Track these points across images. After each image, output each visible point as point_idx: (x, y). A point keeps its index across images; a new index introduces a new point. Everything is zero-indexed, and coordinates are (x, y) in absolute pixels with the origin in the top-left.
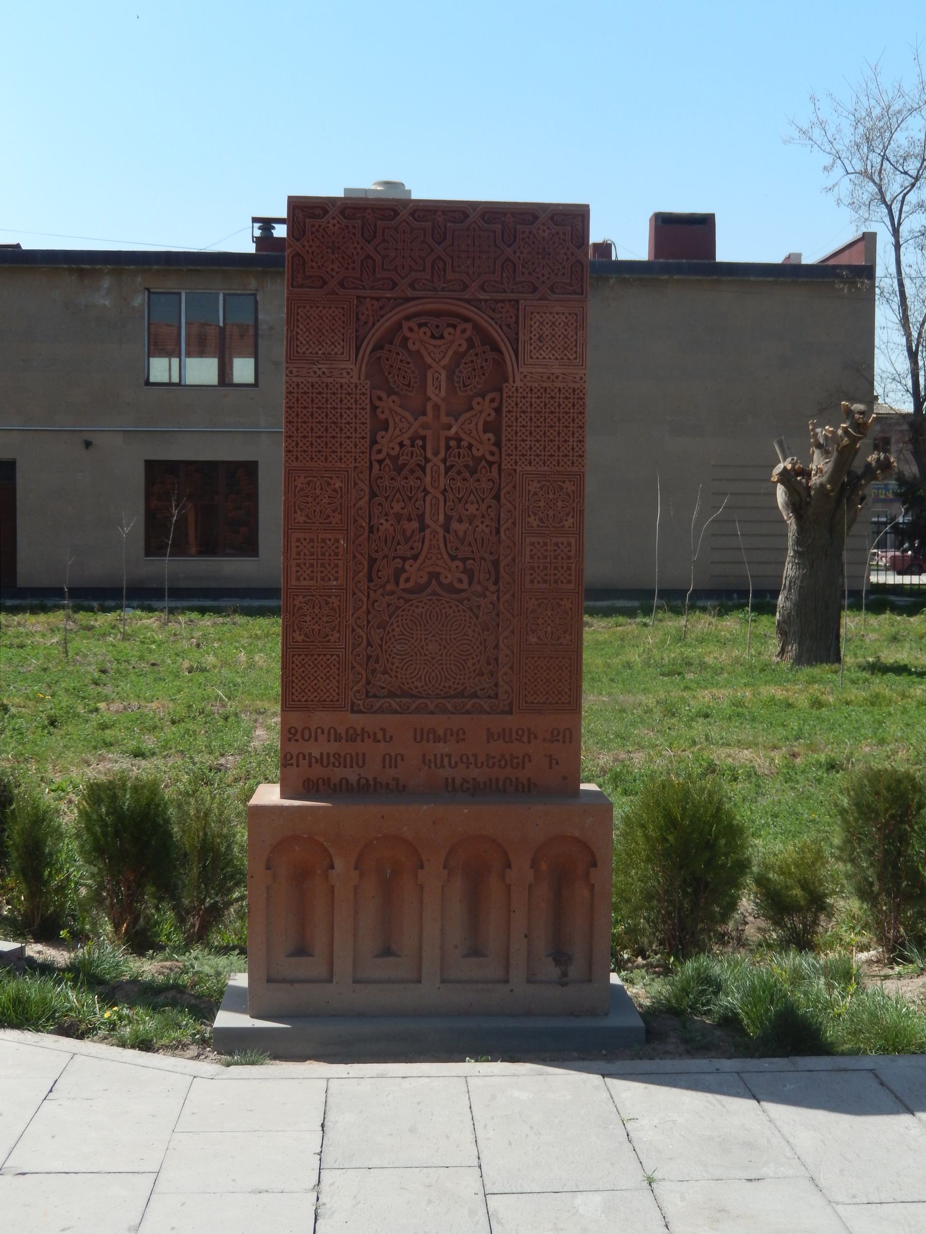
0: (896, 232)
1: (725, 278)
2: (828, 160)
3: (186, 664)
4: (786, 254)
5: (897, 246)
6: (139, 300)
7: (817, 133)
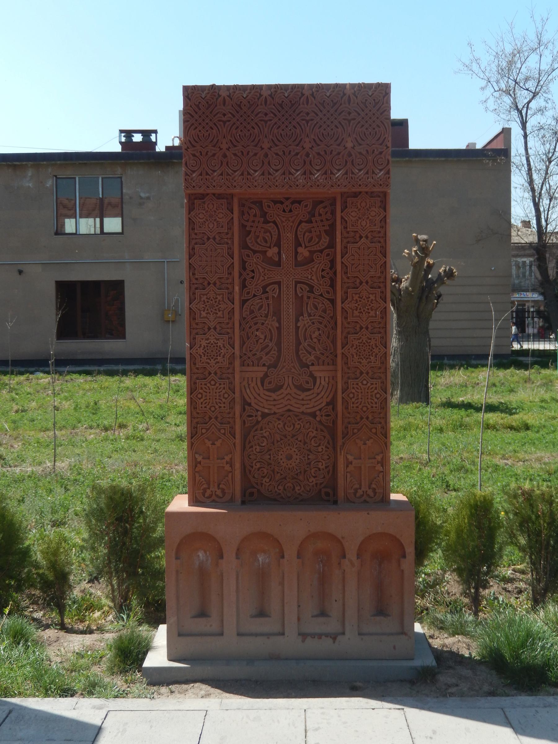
0: (524, 125)
1: (414, 159)
2: (484, 83)
3: (15, 408)
4: (467, 144)
5: (525, 136)
6: (50, 183)
7: (475, 67)
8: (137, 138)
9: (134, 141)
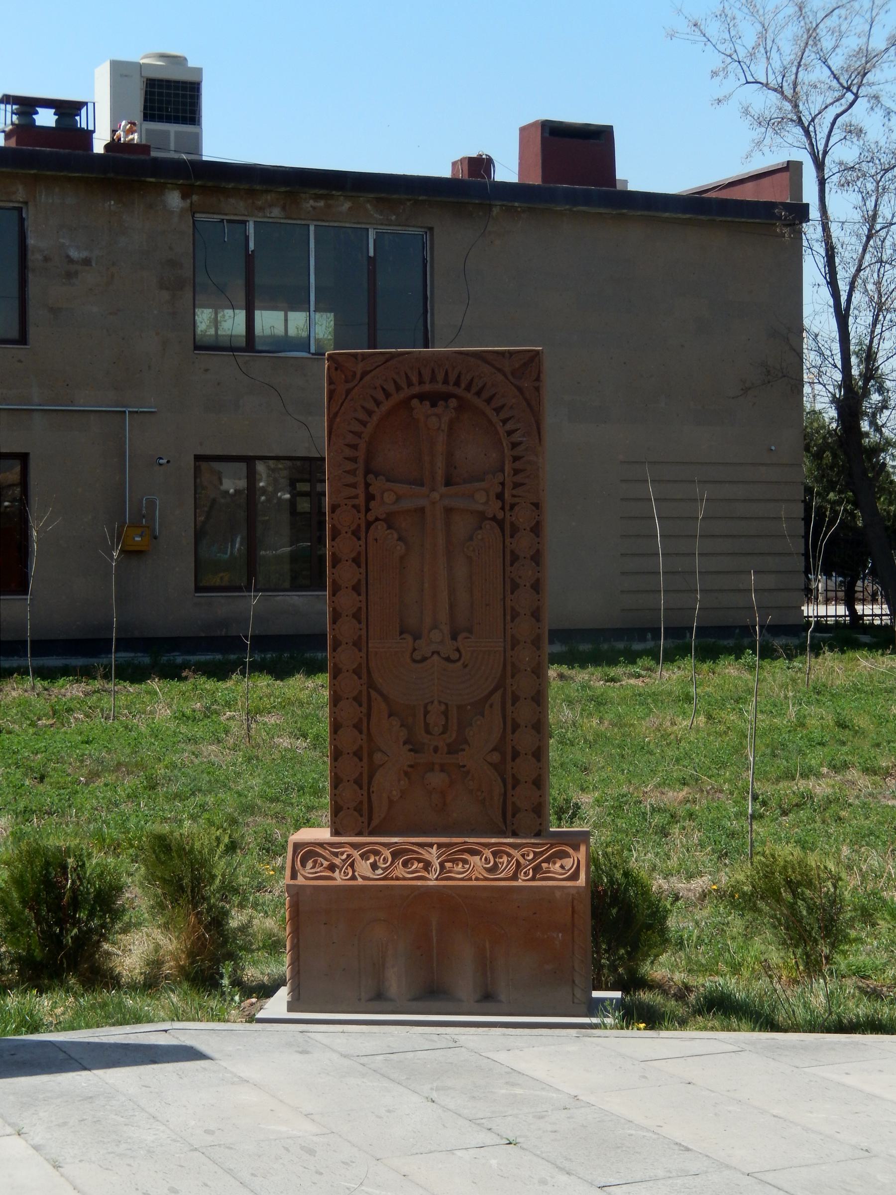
2: (716, 61)
8: (46, 118)
9: (38, 123)
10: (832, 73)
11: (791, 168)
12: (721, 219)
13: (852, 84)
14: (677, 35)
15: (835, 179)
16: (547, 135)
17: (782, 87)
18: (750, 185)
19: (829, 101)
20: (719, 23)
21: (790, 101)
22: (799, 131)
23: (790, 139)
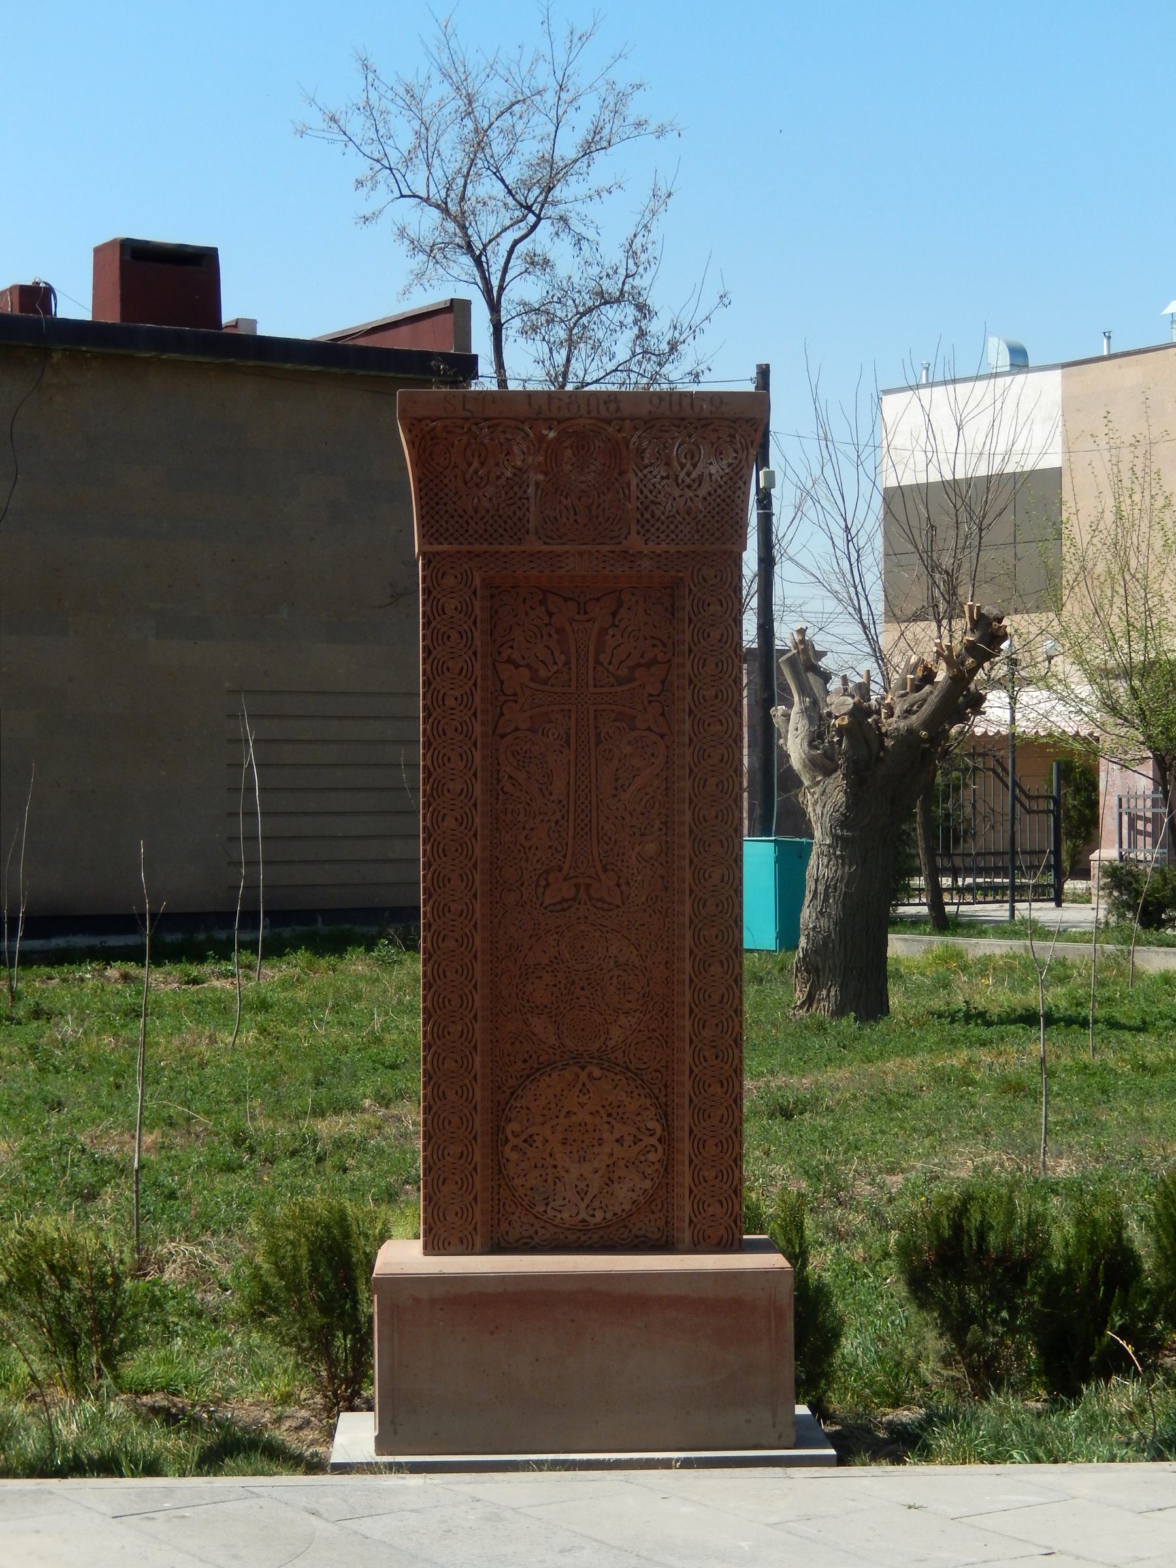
2: (363, 168)
10: (507, 187)
11: (455, 308)
12: (362, 373)
13: (534, 203)
14: (309, 132)
15: (517, 323)
16: (128, 257)
17: (446, 203)
18: (405, 330)
19: (508, 222)
20: (362, 117)
21: (455, 220)
22: (467, 261)
23: (455, 270)
